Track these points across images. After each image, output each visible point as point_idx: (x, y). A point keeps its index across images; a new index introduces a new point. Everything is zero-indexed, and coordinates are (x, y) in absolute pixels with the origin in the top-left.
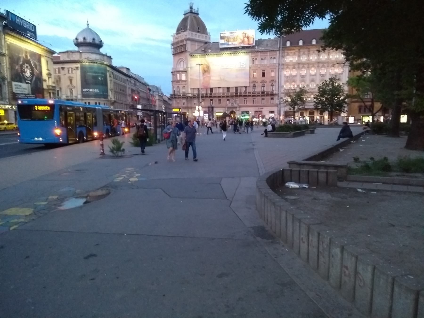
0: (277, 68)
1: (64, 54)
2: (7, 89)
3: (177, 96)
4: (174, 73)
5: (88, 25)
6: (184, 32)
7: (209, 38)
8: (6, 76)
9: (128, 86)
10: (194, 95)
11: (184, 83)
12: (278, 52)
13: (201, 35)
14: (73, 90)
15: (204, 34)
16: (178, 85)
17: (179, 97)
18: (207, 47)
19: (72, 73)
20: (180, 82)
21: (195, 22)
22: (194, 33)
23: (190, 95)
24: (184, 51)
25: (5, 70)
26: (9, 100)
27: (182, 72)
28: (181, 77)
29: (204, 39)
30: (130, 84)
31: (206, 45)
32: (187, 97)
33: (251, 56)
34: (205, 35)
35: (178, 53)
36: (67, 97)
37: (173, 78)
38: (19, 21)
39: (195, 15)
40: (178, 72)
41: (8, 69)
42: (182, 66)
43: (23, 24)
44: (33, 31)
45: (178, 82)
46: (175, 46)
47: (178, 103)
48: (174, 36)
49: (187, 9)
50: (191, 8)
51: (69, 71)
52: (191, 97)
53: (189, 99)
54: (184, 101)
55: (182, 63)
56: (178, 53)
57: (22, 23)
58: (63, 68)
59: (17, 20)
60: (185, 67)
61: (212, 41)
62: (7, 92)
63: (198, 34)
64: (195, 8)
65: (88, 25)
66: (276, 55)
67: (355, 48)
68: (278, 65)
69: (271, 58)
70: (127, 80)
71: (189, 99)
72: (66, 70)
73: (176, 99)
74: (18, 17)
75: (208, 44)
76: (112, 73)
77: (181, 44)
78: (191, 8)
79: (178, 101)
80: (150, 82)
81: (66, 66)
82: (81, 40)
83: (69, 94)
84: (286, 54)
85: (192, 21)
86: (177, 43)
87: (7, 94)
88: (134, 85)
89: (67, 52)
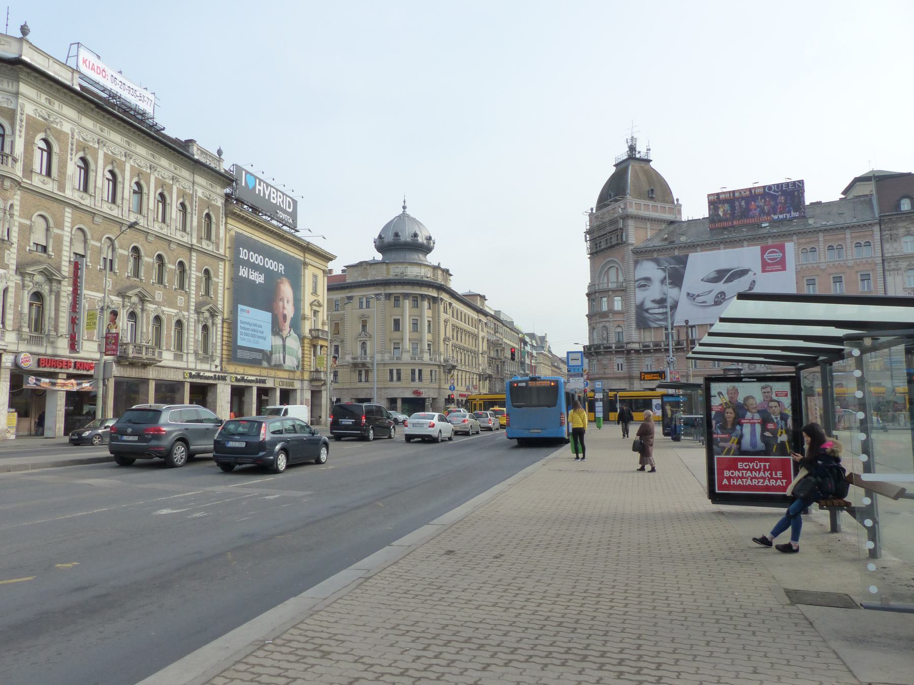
0: (879, 269)
1: (354, 269)
2: (219, 337)
3: (602, 350)
4: (593, 297)
5: (404, 208)
6: (617, 201)
7: (680, 212)
8: (220, 306)
9: (481, 334)
10: (644, 346)
11: (619, 318)
12: (876, 229)
13: (659, 205)
14: (368, 343)
15: (664, 201)
16: (604, 324)
17: (608, 350)
18: (673, 232)
19: (368, 307)
20: (611, 315)
21: (643, 178)
22: (643, 202)
23: (636, 346)
24: (618, 244)
25: (220, 291)
26: (222, 361)
27: (614, 291)
28: (611, 303)
29: (669, 216)
30: (485, 329)
31: (672, 227)
32: (629, 352)
33: (799, 244)
34: (667, 206)
35: (603, 250)
36: (354, 358)
37: (591, 307)
38: (261, 188)
39: (643, 164)
40: (605, 292)
41: (226, 291)
42: (613, 278)
43: (269, 195)
44: (290, 210)
45: (604, 315)
46: (596, 235)
47: (605, 367)
48: (591, 215)
49: (622, 153)
50: (632, 149)
51: (361, 303)
52: (637, 351)
53: (634, 356)
54: (620, 360)
55: (612, 272)
56: (603, 250)
57: (267, 193)
58: (350, 298)
59: (258, 187)
60: (621, 279)
61: (685, 217)
62: (219, 344)
63: (651, 203)
64: (641, 149)
65: (404, 208)
66: (872, 236)
67: (497, 386)
68: (879, 261)
69: (858, 245)
70: (480, 320)
71: (634, 356)
72: (356, 302)
73: (600, 357)
74: (260, 180)
75: (676, 225)
76: (450, 304)
77: (608, 229)
78: (632, 149)
79: (605, 362)
80: (524, 327)
81: (357, 293)
82: (389, 238)
83: (359, 351)
84: (902, 231)
85: (636, 175)
86: (600, 228)
87: (219, 348)
88: (492, 332)
89: (361, 264)
